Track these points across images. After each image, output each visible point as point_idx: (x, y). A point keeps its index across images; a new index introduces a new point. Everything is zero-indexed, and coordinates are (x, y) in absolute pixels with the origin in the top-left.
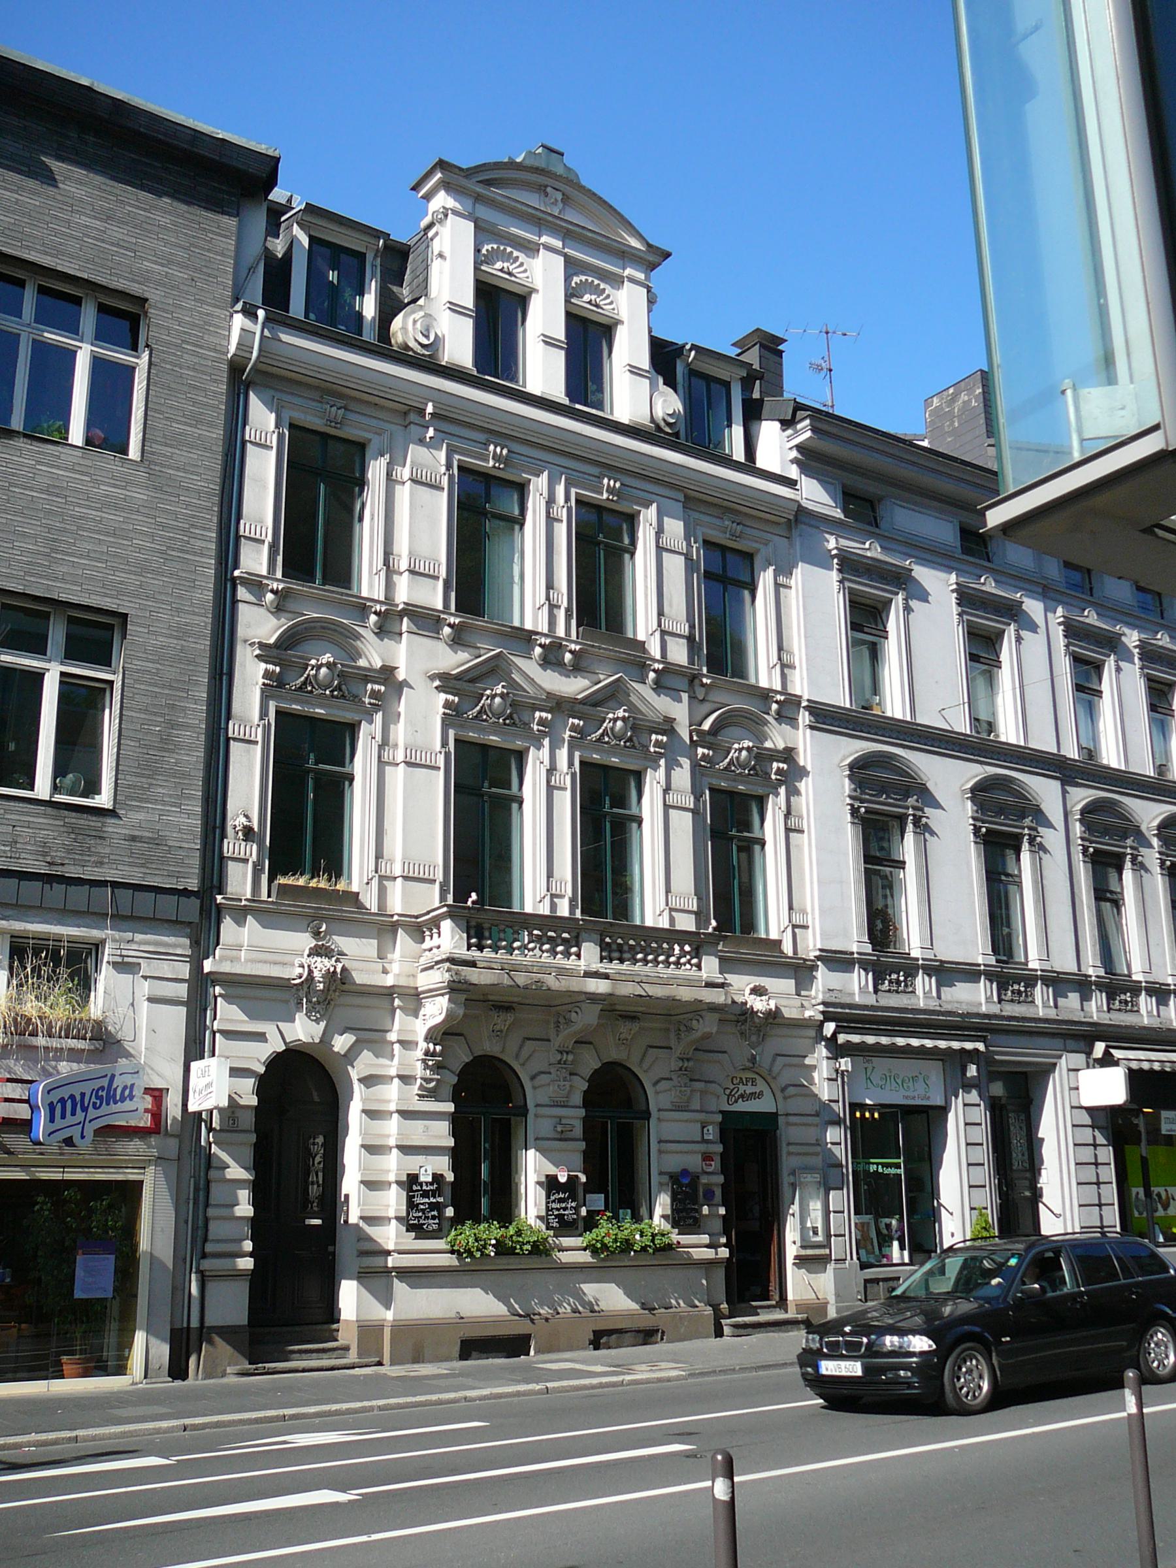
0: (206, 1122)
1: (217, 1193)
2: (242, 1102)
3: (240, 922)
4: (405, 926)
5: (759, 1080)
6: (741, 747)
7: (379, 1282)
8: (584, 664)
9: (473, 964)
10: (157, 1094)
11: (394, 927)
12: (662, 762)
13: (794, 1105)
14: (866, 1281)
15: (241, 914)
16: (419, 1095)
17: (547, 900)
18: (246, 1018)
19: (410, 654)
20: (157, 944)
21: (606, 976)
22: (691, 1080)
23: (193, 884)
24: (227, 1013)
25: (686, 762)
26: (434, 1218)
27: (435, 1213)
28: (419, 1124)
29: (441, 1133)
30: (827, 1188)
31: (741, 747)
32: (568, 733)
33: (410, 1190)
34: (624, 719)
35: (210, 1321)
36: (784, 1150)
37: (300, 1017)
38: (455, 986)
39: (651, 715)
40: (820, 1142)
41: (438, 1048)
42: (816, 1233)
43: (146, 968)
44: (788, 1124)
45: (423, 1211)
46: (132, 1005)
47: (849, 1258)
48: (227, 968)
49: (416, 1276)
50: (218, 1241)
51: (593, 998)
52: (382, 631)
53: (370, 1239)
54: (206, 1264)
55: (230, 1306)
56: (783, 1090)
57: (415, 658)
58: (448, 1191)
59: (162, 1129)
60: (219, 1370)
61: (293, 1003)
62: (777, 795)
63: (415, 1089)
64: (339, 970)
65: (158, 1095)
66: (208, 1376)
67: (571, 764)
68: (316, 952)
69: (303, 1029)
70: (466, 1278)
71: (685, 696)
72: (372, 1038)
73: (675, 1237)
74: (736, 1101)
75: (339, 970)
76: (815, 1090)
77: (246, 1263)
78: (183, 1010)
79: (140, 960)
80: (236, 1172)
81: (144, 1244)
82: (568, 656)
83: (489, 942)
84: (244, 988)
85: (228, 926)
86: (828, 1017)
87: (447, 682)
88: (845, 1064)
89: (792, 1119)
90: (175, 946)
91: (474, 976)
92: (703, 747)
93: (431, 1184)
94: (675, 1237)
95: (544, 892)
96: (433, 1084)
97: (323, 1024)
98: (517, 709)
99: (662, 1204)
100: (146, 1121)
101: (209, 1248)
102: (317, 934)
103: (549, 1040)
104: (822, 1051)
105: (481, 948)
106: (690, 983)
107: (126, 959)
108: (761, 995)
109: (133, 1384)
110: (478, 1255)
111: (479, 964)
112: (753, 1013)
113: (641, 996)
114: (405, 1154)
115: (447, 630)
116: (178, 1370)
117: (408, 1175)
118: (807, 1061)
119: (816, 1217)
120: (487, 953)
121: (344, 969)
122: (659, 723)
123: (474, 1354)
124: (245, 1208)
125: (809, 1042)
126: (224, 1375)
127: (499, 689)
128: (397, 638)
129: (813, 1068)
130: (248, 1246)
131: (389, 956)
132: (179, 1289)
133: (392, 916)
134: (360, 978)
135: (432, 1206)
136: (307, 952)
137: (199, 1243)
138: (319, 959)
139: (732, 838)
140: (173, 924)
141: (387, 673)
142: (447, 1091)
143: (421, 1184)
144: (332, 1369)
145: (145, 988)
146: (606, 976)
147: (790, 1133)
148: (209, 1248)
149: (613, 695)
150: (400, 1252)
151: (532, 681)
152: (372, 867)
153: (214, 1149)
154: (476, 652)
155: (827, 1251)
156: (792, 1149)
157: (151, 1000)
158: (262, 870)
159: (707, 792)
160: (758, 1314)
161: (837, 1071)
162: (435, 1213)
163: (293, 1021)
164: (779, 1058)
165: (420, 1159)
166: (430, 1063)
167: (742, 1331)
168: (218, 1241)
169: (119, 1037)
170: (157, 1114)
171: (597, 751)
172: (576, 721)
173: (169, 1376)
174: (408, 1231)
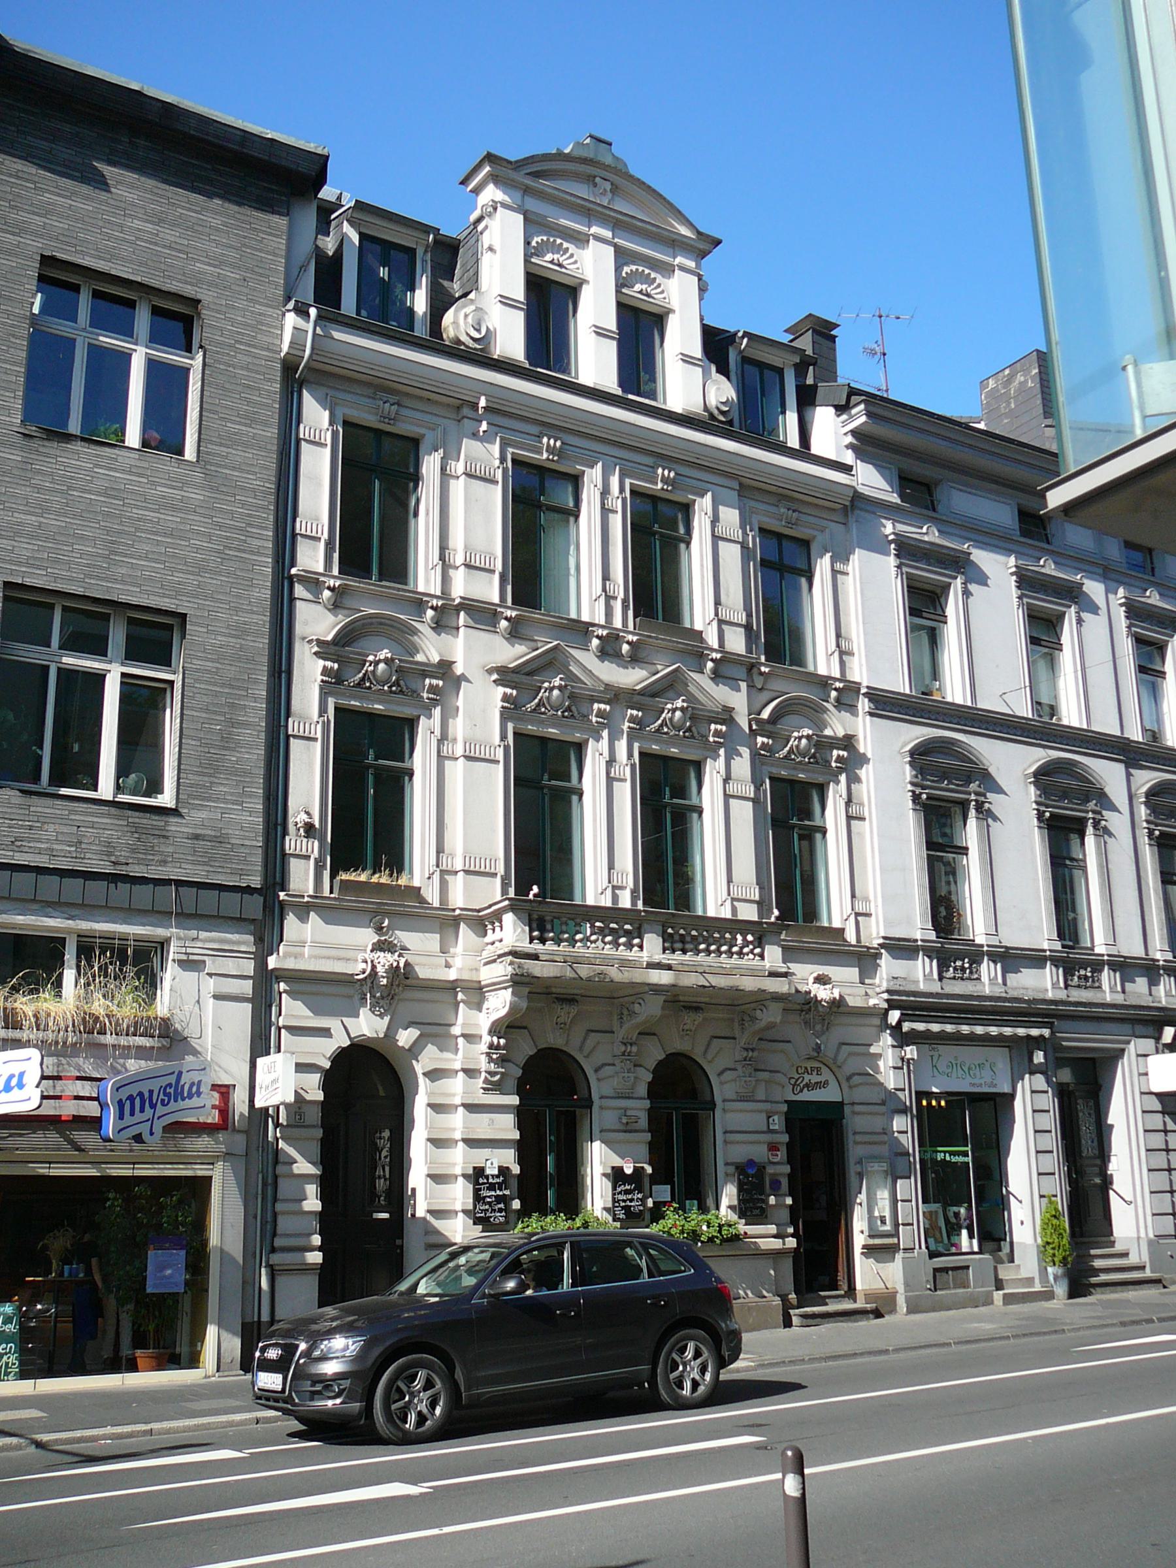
1: (285, 1188)
2: (308, 1097)
3: (303, 918)
5: (824, 1069)
6: (800, 736)
8: (642, 654)
9: (535, 957)
10: (224, 1090)
11: (455, 922)
12: (722, 752)
13: (861, 1094)
14: (936, 1270)
15: (303, 910)
16: (484, 1089)
17: (609, 892)
19: (468, 648)
21: (669, 967)
22: (756, 1070)
23: (256, 881)
24: (292, 1010)
25: (745, 752)
26: (500, 1210)
27: (502, 1206)
28: (485, 1117)
29: (506, 1126)
30: (895, 1176)
31: (800, 736)
32: (627, 724)
33: (476, 1183)
34: (682, 709)
36: (850, 1139)
37: (364, 1012)
39: (710, 705)
40: (887, 1131)
41: (502, 1041)
42: (883, 1222)
44: (854, 1113)
45: (490, 1203)
46: (198, 1002)
47: (917, 1246)
48: (290, 964)
51: (656, 989)
52: (439, 626)
54: (276, 1259)
56: (849, 1079)
57: (474, 653)
61: (357, 997)
62: (838, 782)
63: (480, 1082)
64: (402, 965)
65: (224, 1091)
67: (630, 755)
68: (379, 947)
69: (367, 1024)
71: (743, 685)
72: (436, 1032)
73: (742, 1227)
74: (801, 1091)
75: (402, 965)
76: (881, 1078)
77: (315, 1257)
78: (248, 1007)
79: (205, 958)
80: (304, 1167)
81: (214, 1240)
82: (625, 648)
84: (310, 985)
86: (892, 1005)
87: (505, 676)
88: (911, 1052)
89: (857, 1108)
90: (239, 943)
91: (537, 969)
92: (762, 736)
93: (498, 1176)
94: (742, 1227)
95: (850, 911)
97: (387, 1019)
98: (576, 700)
99: (729, 1195)
100: (213, 1117)
101: (278, 1242)
102: (379, 929)
103: (734, 1038)
104: (887, 1039)
105: (543, 941)
106: (753, 973)
107: (191, 957)
108: (825, 984)
109: (206, 1377)
111: (542, 957)
112: (817, 1001)
113: (704, 987)
115: (504, 624)
117: (475, 1168)
118: (873, 1050)
119: (883, 1206)
120: (550, 946)
121: (407, 964)
122: (718, 713)
124: (313, 1203)
125: (874, 1030)
127: (557, 682)
128: (454, 632)
129: (879, 1056)
130: (316, 1240)
131: (452, 950)
132: (249, 1282)
133: (454, 910)
135: (499, 1199)
136: (370, 947)
139: (793, 827)
140: (237, 922)
141: (445, 668)
142: (512, 1084)
143: (487, 1177)
145: (210, 985)
146: (669, 967)
147: (857, 1122)
148: (278, 1242)
149: (671, 686)
151: (590, 673)
152: (433, 861)
154: (533, 644)
155: (895, 1240)
156: (858, 1138)
159: (768, 781)
160: (826, 1304)
161: (902, 1059)
162: (502, 1206)
163: (357, 1016)
164: (844, 1047)
165: (486, 1152)
166: (495, 1056)
167: (810, 1321)
170: (224, 1110)
171: (657, 742)
172: (635, 712)
174: (475, 1224)
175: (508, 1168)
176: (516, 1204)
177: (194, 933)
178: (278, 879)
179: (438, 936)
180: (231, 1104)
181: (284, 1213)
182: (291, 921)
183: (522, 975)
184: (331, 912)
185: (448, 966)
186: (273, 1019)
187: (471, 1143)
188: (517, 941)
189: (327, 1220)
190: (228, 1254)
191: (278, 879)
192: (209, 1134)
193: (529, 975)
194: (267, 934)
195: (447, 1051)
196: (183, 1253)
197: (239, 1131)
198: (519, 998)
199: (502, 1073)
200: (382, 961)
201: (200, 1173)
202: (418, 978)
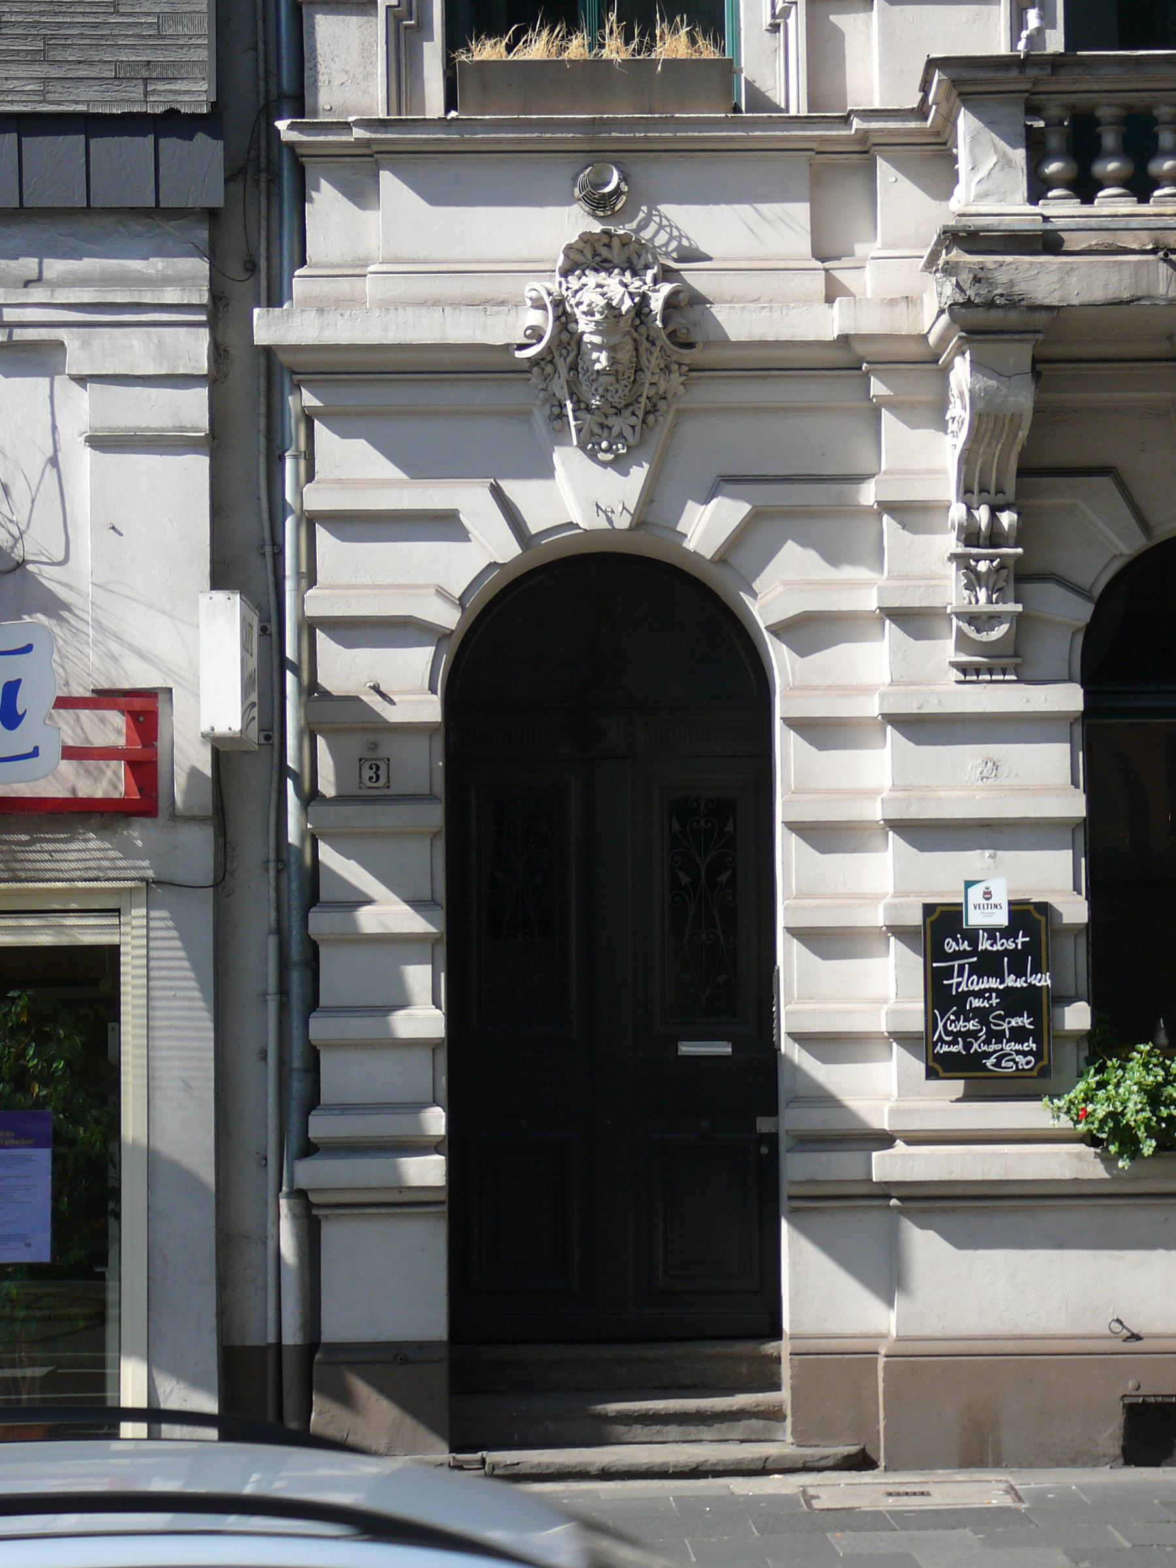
0: (297, 779)
1: (338, 976)
2: (393, 715)
3: (362, 193)
4: (894, 146)
7: (863, 1224)
9: (1047, 242)
10: (138, 704)
11: (863, 155)
15: (358, 166)
16: (963, 668)
18: (403, 476)
20: (83, 281)
23: (194, 93)
24: (347, 467)
26: (1019, 1035)
27: (1024, 1021)
28: (967, 758)
29: (1045, 779)
33: (934, 951)
35: (334, 1329)
37: (567, 460)
41: (1007, 519)
43: (81, 352)
45: (982, 1015)
46: (54, 461)
49: (979, 1211)
50: (344, 1108)
53: (826, 1100)
54: (308, 1172)
55: (394, 1286)
58: (1076, 960)
59: (163, 803)
63: (946, 650)
64: (657, 304)
65: (143, 710)
68: (588, 256)
69: (581, 494)
70: (1145, 1217)
72: (808, 500)
75: (657, 304)
77: (427, 1171)
78: (198, 466)
79: (62, 334)
80: (389, 913)
81: (132, 1126)
83: (1112, 166)
84: (397, 388)
90: (165, 281)
91: (1042, 280)
93: (1008, 932)
97: (639, 474)
100: (110, 782)
101: (320, 1127)
102: (600, 204)
105: (1085, 188)
107: (20, 334)
111: (1073, 241)
117: (928, 909)
120: (1111, 203)
124: (423, 1018)
130: (436, 1121)
131: (860, 249)
132: (234, 1243)
133: (845, 120)
134: (739, 322)
135: (1013, 1001)
137: (295, 1117)
140: (150, 220)
142: (1062, 640)
143: (972, 936)
145: (81, 410)
148: (320, 1127)
150: (914, 1139)
153: (328, 855)
157: (101, 442)
158: (423, 28)
162: (1024, 1021)
163: (546, 471)
165: (974, 861)
166: (983, 566)
168: (344, 1108)
169: (17, 554)
170: (145, 766)
174: (931, 1074)
176: (1077, 1017)
177: (28, 266)
179: (801, 211)
180: (162, 744)
182: (326, 208)
183: (990, 304)
184: (447, 163)
187: (925, 833)
188: (982, 196)
189: (471, 1057)
192: (102, 830)
193: (1012, 303)
194: (251, 241)
195: (852, 560)
196: (44, 1156)
200: (591, 296)
202: (725, 342)
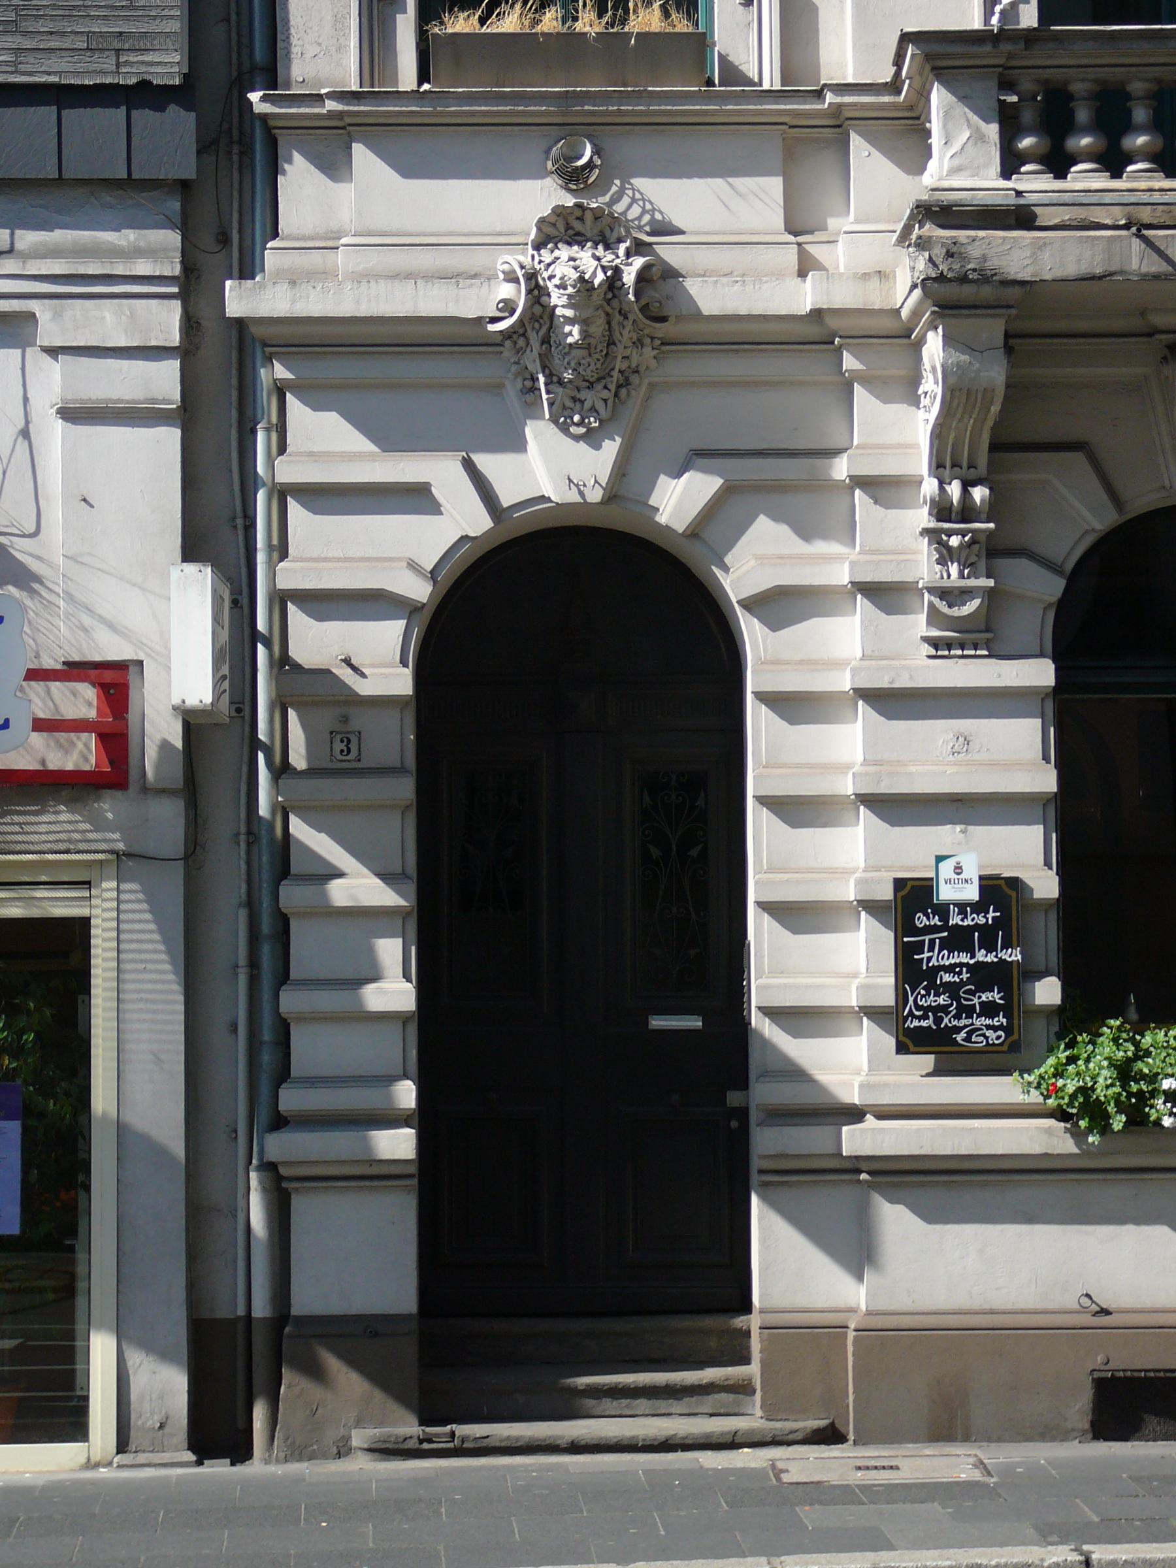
1: (309, 948)
2: (365, 688)
3: (334, 166)
4: (868, 121)
7: (833, 1199)
9: (1020, 217)
10: (109, 676)
11: (837, 128)
15: (333, 138)
16: (935, 643)
20: (55, 253)
23: (167, 65)
24: (319, 440)
26: (989, 1010)
27: (995, 996)
28: (939, 733)
29: (1016, 754)
37: (540, 434)
38: (951, 291)
41: (979, 494)
46: (25, 433)
48: (315, 303)
53: (797, 1074)
54: (278, 1146)
58: (1047, 935)
59: (133, 774)
60: (331, 1435)
61: (512, 391)
63: (918, 624)
64: (629, 277)
65: (114, 682)
66: (297, 1453)
68: (561, 229)
69: (552, 467)
70: (1118, 1192)
72: (782, 475)
75: (629, 277)
77: (397, 1144)
79: (34, 306)
80: (359, 886)
85: (300, 186)
91: (1015, 255)
93: (979, 907)
96: (971, 607)
97: (611, 448)
100: (80, 754)
101: (290, 1100)
102: (573, 177)
105: (1058, 163)
109: (90, 1465)
110: (1118, 1122)
111: (1046, 216)
114: (894, 822)
116: (217, 1431)
117: (899, 884)
120: (1084, 178)
123: (1152, 1422)
124: (394, 991)
126: (343, 1450)
130: (406, 1094)
131: (833, 223)
133: (819, 94)
134: (712, 296)
135: (984, 976)
137: (265, 1090)
138: (564, 252)
140: (123, 192)
143: (942, 910)
144: (666, 1446)
145: (53, 381)
148: (290, 1100)
153: (299, 828)
162: (995, 996)
163: (518, 445)
165: (945, 836)
166: (954, 541)
170: (115, 737)
173: (191, 1448)
174: (901, 1049)
175: (1015, 883)
176: (1048, 992)
178: (259, 54)
179: (774, 186)
180: (132, 717)
181: (303, 1019)
183: (963, 279)
184: (419, 136)
185: (805, 266)
186: (260, 469)
190: (145, 1139)
191: (259, 54)
192: (73, 802)
193: (986, 278)
195: (826, 536)
197: (161, 792)
198: (970, 349)
199: (990, 593)
200: (563, 270)
201: (59, 911)
202: (698, 316)
